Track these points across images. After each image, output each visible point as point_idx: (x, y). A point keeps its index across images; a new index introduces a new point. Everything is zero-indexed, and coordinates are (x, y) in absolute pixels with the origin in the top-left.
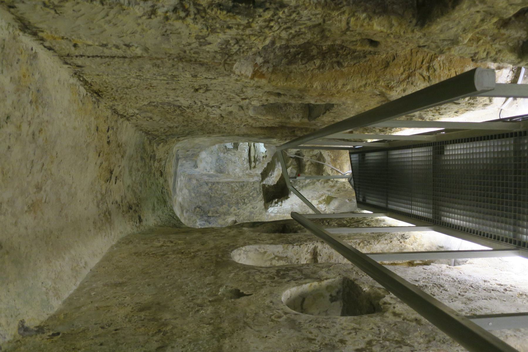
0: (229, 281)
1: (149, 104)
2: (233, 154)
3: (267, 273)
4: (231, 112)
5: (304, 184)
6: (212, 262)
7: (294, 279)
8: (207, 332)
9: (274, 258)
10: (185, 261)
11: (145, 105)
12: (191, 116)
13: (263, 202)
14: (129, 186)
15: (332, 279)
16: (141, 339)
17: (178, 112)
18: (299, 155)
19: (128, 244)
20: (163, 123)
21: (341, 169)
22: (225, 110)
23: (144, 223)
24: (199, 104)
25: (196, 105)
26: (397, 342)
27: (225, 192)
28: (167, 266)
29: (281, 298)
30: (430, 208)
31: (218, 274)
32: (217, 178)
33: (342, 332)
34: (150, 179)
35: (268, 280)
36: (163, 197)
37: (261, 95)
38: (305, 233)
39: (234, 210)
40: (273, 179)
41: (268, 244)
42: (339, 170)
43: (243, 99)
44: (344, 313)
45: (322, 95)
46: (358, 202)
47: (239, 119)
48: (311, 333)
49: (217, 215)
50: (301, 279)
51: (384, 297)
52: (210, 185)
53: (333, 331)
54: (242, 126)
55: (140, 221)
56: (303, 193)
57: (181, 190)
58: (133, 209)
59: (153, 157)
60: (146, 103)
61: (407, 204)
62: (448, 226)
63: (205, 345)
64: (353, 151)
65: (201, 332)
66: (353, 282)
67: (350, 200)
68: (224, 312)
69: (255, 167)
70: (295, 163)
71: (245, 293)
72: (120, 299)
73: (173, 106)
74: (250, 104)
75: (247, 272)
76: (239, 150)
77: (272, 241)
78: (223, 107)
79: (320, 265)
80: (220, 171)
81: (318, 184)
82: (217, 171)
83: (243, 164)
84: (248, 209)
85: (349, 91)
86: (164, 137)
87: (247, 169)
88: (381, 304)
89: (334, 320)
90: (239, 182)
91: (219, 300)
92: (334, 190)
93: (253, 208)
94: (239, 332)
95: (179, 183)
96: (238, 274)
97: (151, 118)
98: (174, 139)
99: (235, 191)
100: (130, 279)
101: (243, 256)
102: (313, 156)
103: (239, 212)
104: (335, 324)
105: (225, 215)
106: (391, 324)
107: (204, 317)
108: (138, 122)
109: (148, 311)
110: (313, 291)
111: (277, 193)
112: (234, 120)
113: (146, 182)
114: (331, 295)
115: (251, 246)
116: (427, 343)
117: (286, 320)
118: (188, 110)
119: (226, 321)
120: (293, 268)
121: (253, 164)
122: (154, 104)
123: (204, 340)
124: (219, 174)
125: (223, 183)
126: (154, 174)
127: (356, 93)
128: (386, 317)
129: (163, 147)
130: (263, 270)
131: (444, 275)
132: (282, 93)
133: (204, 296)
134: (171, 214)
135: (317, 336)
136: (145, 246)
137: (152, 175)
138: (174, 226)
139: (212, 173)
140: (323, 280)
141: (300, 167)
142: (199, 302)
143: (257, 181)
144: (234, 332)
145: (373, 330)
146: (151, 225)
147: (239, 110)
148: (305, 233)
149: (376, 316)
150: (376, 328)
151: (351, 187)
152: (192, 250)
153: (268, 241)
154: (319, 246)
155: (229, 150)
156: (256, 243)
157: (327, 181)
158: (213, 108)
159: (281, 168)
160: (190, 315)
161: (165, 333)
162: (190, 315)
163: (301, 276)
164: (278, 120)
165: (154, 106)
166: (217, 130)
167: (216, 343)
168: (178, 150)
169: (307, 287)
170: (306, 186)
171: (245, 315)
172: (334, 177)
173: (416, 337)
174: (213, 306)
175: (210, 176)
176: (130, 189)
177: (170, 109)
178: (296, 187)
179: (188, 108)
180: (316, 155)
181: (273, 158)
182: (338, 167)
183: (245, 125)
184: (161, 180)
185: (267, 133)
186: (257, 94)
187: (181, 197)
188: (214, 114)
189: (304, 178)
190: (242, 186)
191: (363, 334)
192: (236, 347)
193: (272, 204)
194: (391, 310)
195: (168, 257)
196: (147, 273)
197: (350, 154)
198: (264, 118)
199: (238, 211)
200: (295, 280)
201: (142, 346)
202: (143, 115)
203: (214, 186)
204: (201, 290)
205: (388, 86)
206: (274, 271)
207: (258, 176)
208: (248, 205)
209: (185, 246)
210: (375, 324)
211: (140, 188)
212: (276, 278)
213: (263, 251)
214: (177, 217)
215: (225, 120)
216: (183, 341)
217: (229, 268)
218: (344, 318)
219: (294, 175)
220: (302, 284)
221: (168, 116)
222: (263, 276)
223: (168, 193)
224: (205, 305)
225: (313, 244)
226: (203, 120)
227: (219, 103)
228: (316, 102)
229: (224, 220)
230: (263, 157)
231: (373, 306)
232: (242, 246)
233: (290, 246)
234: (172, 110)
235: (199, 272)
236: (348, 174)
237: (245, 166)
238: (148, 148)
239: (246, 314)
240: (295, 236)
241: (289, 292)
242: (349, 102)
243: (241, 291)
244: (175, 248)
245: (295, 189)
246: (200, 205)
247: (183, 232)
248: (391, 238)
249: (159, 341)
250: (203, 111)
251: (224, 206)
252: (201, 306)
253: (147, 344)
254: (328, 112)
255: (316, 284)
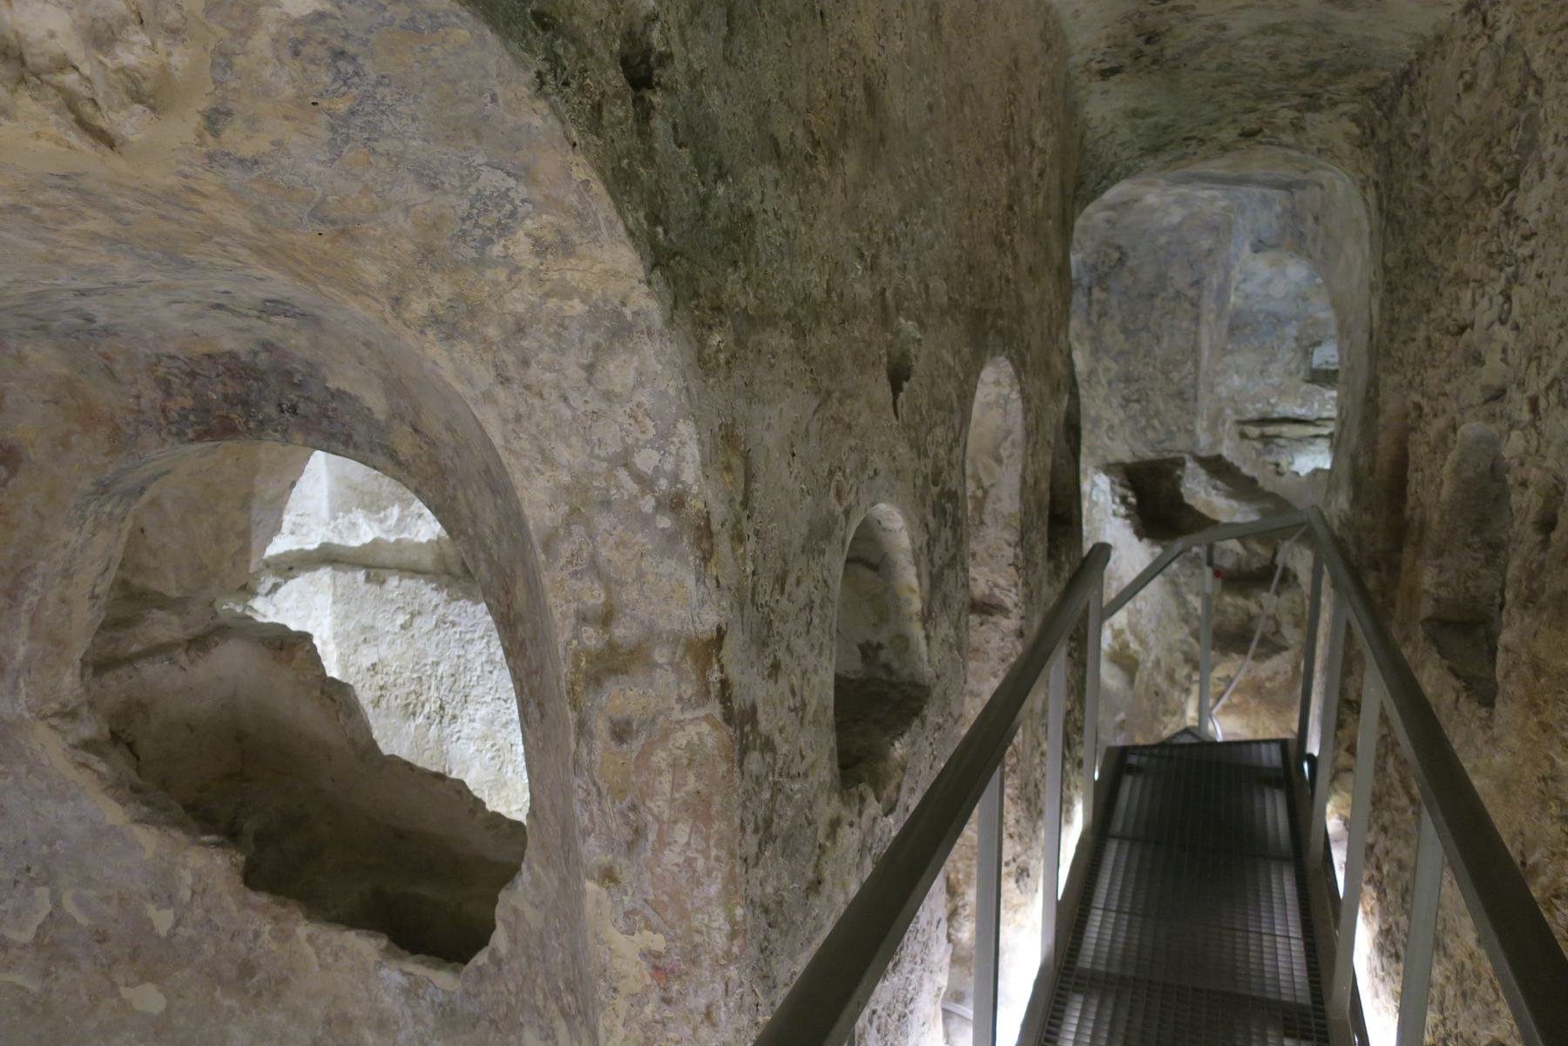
0: (932, 349)
1: (1531, 76)
2: (1293, 366)
3: (950, 463)
4: (1478, 360)
5: (1184, 589)
6: (983, 300)
7: (931, 543)
8: (809, 282)
9: (980, 486)
10: (991, 215)
11: (1527, 62)
12: (1472, 225)
13: (1127, 458)
14: (1224, 28)
15: (926, 655)
16: (799, 90)
17: (1492, 179)
18: (1283, 579)
19: (1043, 38)
20: (1446, 128)
21: (1227, 709)
22: (1490, 340)
23: (1097, 85)
24: (1523, 252)
25: (1517, 239)
26: (768, 822)
27: (1165, 342)
28: (979, 162)
29: (883, 501)
30: (1108, 965)
31: (953, 319)
32: (1212, 317)
33: (798, 671)
34: (1239, 95)
35: (930, 466)
36: (1172, 142)
37: (1548, 463)
38: (1045, 585)
39: (1107, 370)
40: (1200, 491)
41: (1025, 468)
42: (1224, 700)
43: (1534, 404)
44: (841, 683)
45: (1538, 671)
46: (1124, 751)
47: (1448, 388)
48: (798, 583)
49: (1094, 318)
50: (931, 561)
51: (878, 800)
52: (1192, 293)
53: (799, 644)
54: (1416, 398)
55: (1105, 74)
56: (1155, 587)
57: (1182, 201)
58: (1148, 49)
59: (1312, 103)
60: (1535, 66)
61: (1121, 898)
62: (1054, 1009)
63: (779, 278)
64: (1292, 750)
65: (810, 265)
66: (916, 714)
67: (1122, 726)
68: (857, 334)
69: (1243, 436)
70: (1256, 564)
71: (902, 395)
72: (897, 23)
73: (1518, 163)
74: (1511, 427)
75: (955, 404)
76: (1305, 387)
77: (1031, 481)
78: (1504, 334)
79: (963, 620)
80: (1238, 327)
81: (1180, 633)
82: (1238, 313)
83: (1254, 399)
84: (1107, 414)
85: (1545, 763)
86: (1382, 136)
87: (1237, 411)
88: (862, 787)
89: (827, 652)
90: (1195, 386)
91: (885, 321)
92: (1160, 680)
93: (1111, 427)
94: (808, 375)
95: (1206, 194)
96: (949, 375)
97: (1469, 87)
98: (1370, 171)
99: (1166, 374)
100: (948, 52)
101: (994, 390)
102: (1278, 624)
103: (1099, 383)
104: (816, 652)
105: (1093, 339)
106: (811, 808)
107: (845, 273)
108: (1459, 43)
109: (864, 108)
110: (896, 597)
111: (1157, 505)
112: (1443, 372)
113: (1228, 83)
114: (880, 646)
115: (1020, 419)
116: (762, 905)
117: (831, 513)
118: (1496, 214)
119: (835, 339)
120: (959, 541)
121: (1254, 431)
122: (1531, 92)
123: (793, 274)
124: (1226, 322)
125: (1196, 333)
126: (1253, 110)
127: (1541, 785)
128: (829, 799)
129: (1347, 135)
130: (958, 451)
131: (921, 978)
132: (1555, 536)
133: (897, 274)
134: (1117, 170)
135: (789, 599)
136: (1035, 92)
137: (1249, 104)
138: (1081, 181)
139: (1233, 299)
140: (925, 628)
141: (1241, 580)
142: (884, 259)
143: (1196, 443)
144: (808, 363)
145: (798, 759)
146: (1087, 109)
147: (1484, 388)
148: (1045, 585)
149: (831, 770)
150: (802, 767)
151: (1166, 734)
152: (1017, 237)
153: (1030, 468)
154: (1010, 623)
155: (1307, 354)
156: (1028, 433)
157: (1189, 659)
158: (1501, 299)
159: (1238, 519)
160: (851, 235)
161: (810, 160)
162: (851, 235)
163: (938, 562)
164: (1436, 517)
165: (1522, 95)
166: (1404, 313)
167: (782, 310)
168: (1321, 186)
169: (909, 578)
170: (1178, 594)
171: (848, 395)
172: (1203, 685)
173: (779, 877)
174: (872, 302)
175: (1222, 292)
176: (1212, 33)
177: (1509, 151)
178: (1175, 565)
179: (1506, 213)
180: (1277, 632)
181: (1272, 496)
182: (1236, 700)
183: (1418, 407)
184: (1228, 134)
185: (1381, 478)
186: (1553, 449)
187: (1156, 202)
188: (1474, 303)
189: (1209, 588)
190: (1180, 394)
191: (790, 729)
192: (772, 366)
193: (1122, 485)
194: (848, 815)
195: (1001, 165)
196: (962, 102)
197: (1283, 743)
198: (1447, 469)
199: (1104, 381)
200: (928, 544)
201: (781, 94)
202: (1486, 59)
203: (1186, 305)
204: (911, 265)
205: (1557, 897)
206: (953, 485)
207: (1213, 445)
208: (1121, 414)
209: (1029, 214)
210: (812, 765)
211: (1213, 65)
212: (935, 490)
213: (1004, 453)
214: (1106, 188)
215: (1447, 343)
216: (791, 215)
217: (966, 351)
218: (830, 680)
219: (1216, 561)
220: (917, 564)
221: (1475, 146)
222: (942, 452)
223: (1181, 158)
224: (875, 278)
225: (1016, 605)
226: (1453, 266)
227: (1521, 321)
228: (1507, 649)
229: (1078, 338)
230: (1277, 465)
231: (858, 766)
232: (1022, 391)
233: (1013, 537)
234: (1499, 159)
235: (960, 258)
236: (1210, 726)
237: (1249, 406)
238: (1352, 82)
239: (851, 396)
240: (1041, 549)
241: (898, 527)
242: (1498, 758)
243: (906, 385)
244: (1024, 185)
245: (1169, 563)
246: (1129, 264)
247: (1064, 209)
248: (1020, 837)
249: (792, 142)
250: (1492, 265)
251: (1121, 337)
252: (873, 267)
253: (785, 108)
254: (1459, 684)
255: (917, 605)
